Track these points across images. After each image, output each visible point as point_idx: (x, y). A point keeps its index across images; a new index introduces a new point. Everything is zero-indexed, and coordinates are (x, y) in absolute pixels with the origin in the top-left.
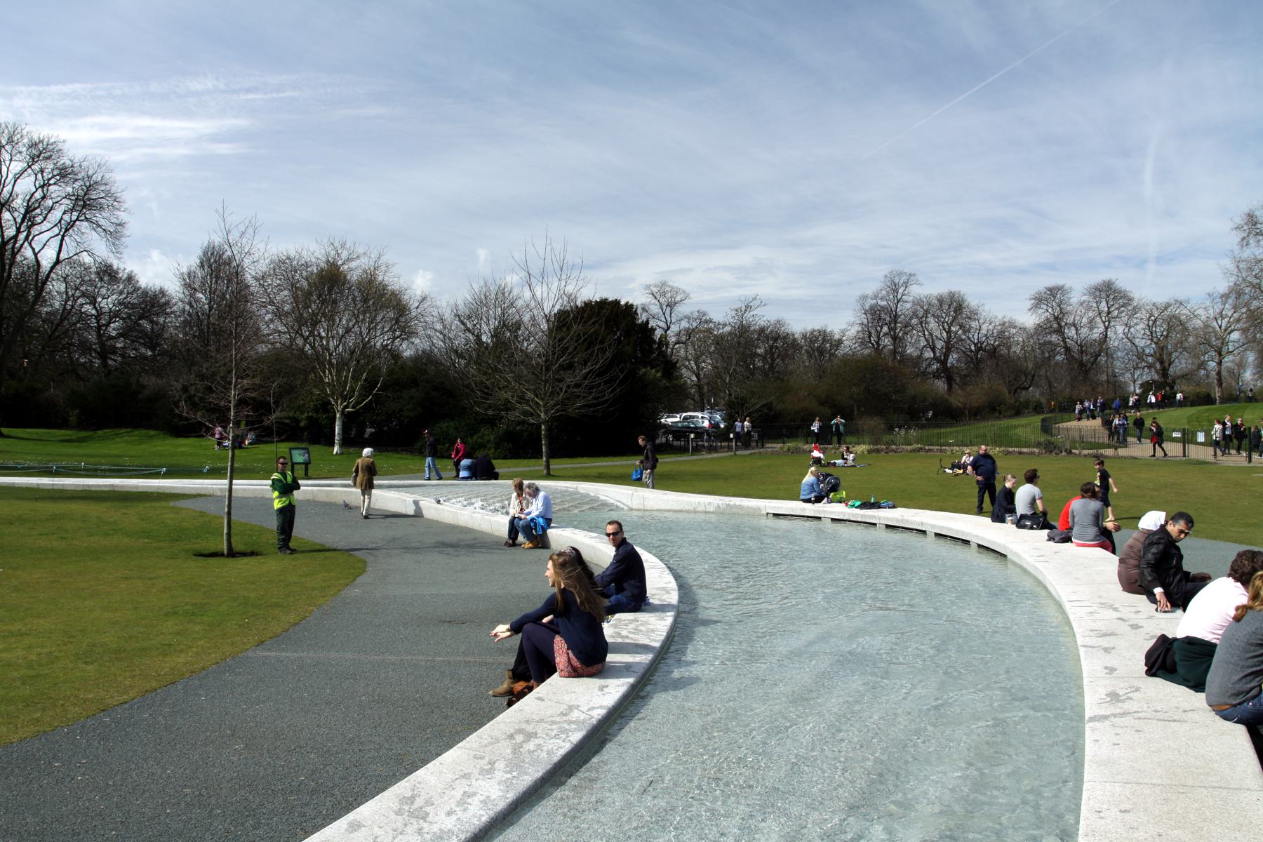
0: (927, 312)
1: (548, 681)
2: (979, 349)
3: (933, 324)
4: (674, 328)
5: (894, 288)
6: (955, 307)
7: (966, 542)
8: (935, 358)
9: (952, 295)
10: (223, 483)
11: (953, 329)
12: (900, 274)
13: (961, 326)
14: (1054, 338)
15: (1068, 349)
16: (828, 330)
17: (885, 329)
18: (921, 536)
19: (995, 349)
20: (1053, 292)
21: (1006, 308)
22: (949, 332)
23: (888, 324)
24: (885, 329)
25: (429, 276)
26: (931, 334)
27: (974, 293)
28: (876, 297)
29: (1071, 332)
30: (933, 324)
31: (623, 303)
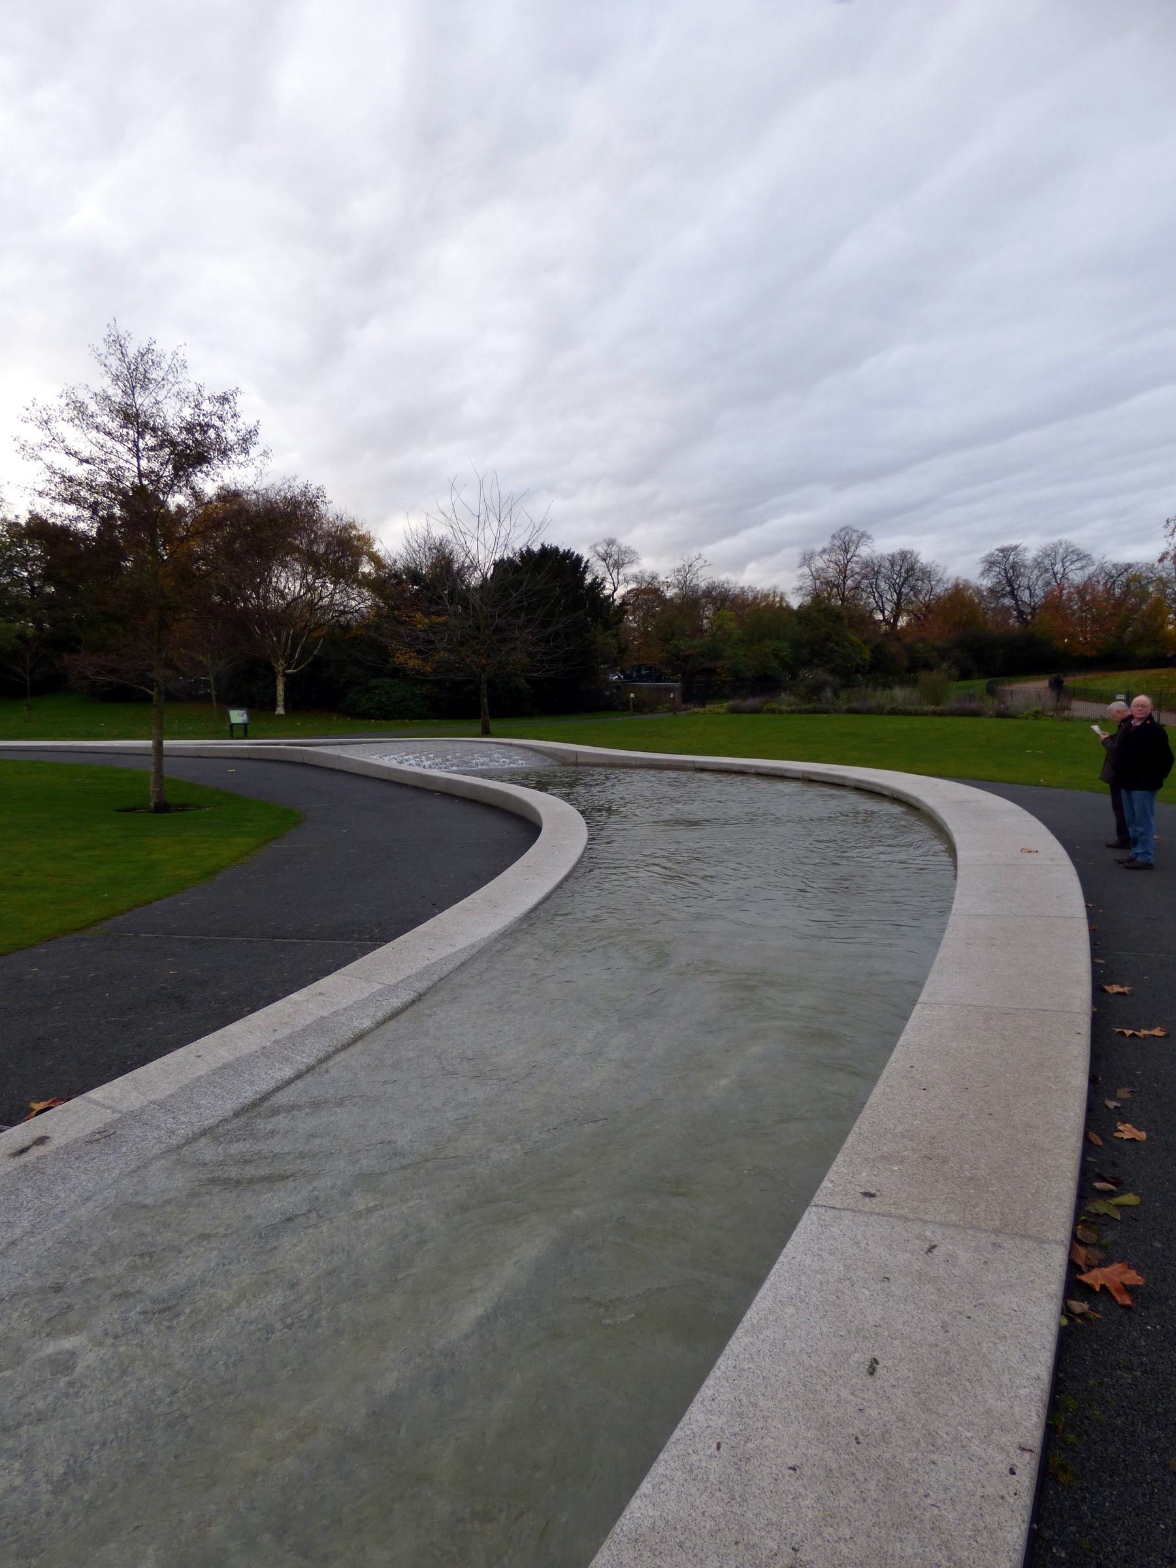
5: (845, 542)
6: (907, 570)
8: (884, 620)
9: (904, 555)
10: (149, 743)
13: (912, 588)
14: (1008, 602)
15: (1021, 613)
18: (19, 1147)
21: (955, 556)
22: (899, 594)
27: (926, 551)
29: (1025, 596)
31: (561, 550)
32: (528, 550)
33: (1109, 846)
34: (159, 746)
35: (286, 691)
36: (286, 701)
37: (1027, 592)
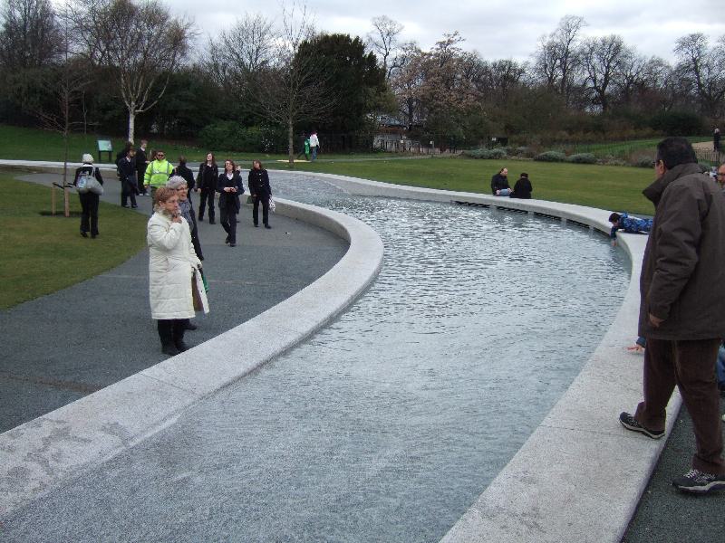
0: (592, 49)
1: (298, 295)
2: (631, 82)
3: (595, 60)
4: (393, 54)
5: (569, 28)
6: (613, 51)
7: (527, 212)
8: (595, 87)
9: (613, 39)
10: (63, 164)
11: (612, 65)
12: (573, 18)
14: (691, 75)
16: (513, 61)
17: (558, 61)
19: (643, 82)
20: (694, 38)
22: (608, 67)
23: (561, 59)
24: (558, 61)
25: (315, 136)
26: (593, 68)
28: (551, 36)
29: (704, 72)
30: (595, 60)
32: (348, 36)
33: (231, 239)
34: (65, 165)
35: (128, 123)
36: (135, 135)
37: (706, 69)
